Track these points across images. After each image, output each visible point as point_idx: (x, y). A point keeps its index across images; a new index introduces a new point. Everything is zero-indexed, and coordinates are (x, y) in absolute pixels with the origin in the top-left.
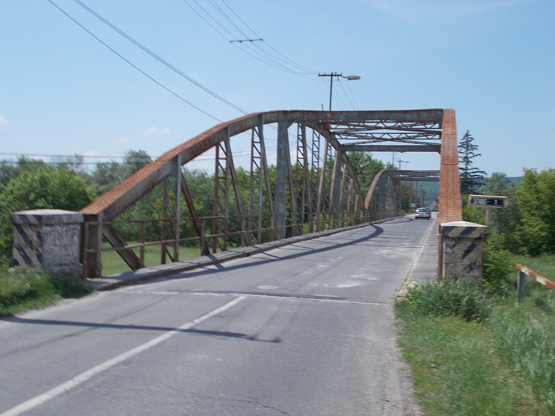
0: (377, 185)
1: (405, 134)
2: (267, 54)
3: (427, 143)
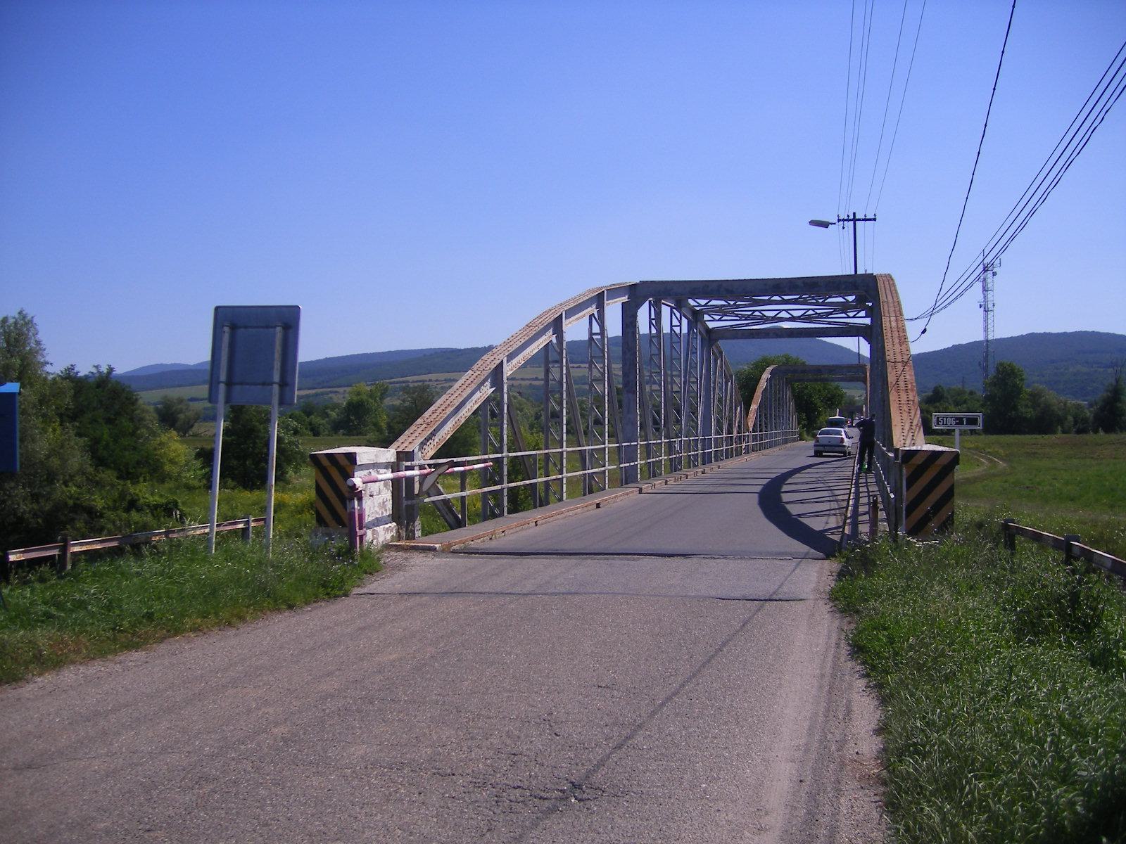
1: (813, 310)
3: (847, 324)
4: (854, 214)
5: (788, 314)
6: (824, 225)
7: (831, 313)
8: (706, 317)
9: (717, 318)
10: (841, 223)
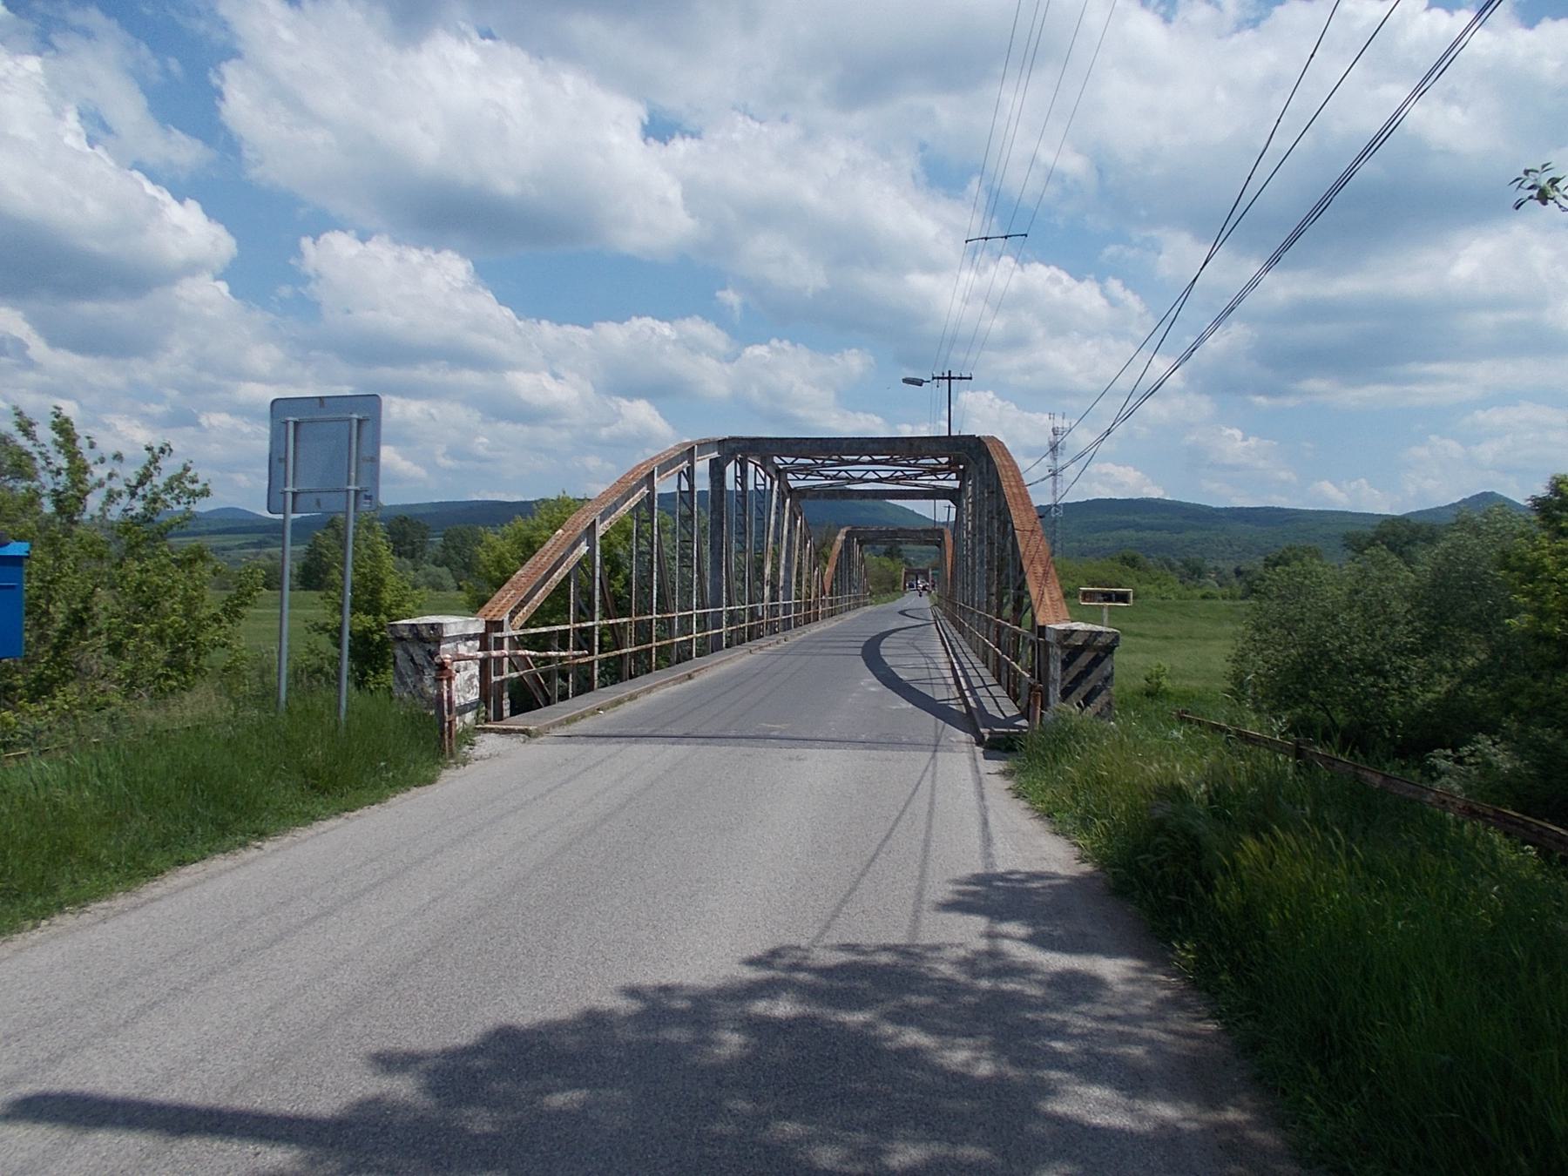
0: (1543, 821)
1: (902, 471)
2: (1182, 299)
3: (934, 486)
4: (950, 372)
5: (869, 475)
6: (919, 383)
7: (921, 475)
8: (790, 476)
9: (802, 477)
10: (936, 380)
